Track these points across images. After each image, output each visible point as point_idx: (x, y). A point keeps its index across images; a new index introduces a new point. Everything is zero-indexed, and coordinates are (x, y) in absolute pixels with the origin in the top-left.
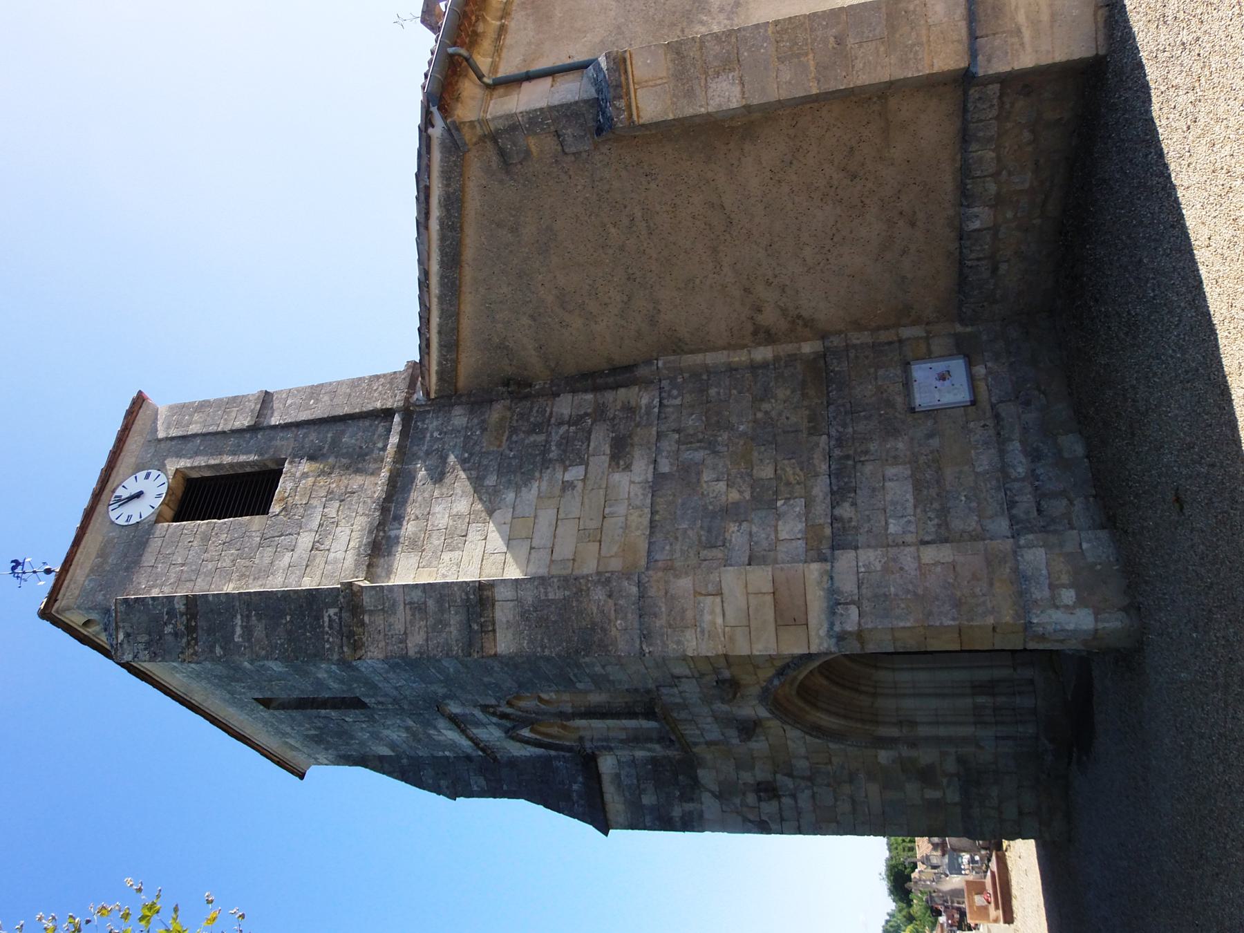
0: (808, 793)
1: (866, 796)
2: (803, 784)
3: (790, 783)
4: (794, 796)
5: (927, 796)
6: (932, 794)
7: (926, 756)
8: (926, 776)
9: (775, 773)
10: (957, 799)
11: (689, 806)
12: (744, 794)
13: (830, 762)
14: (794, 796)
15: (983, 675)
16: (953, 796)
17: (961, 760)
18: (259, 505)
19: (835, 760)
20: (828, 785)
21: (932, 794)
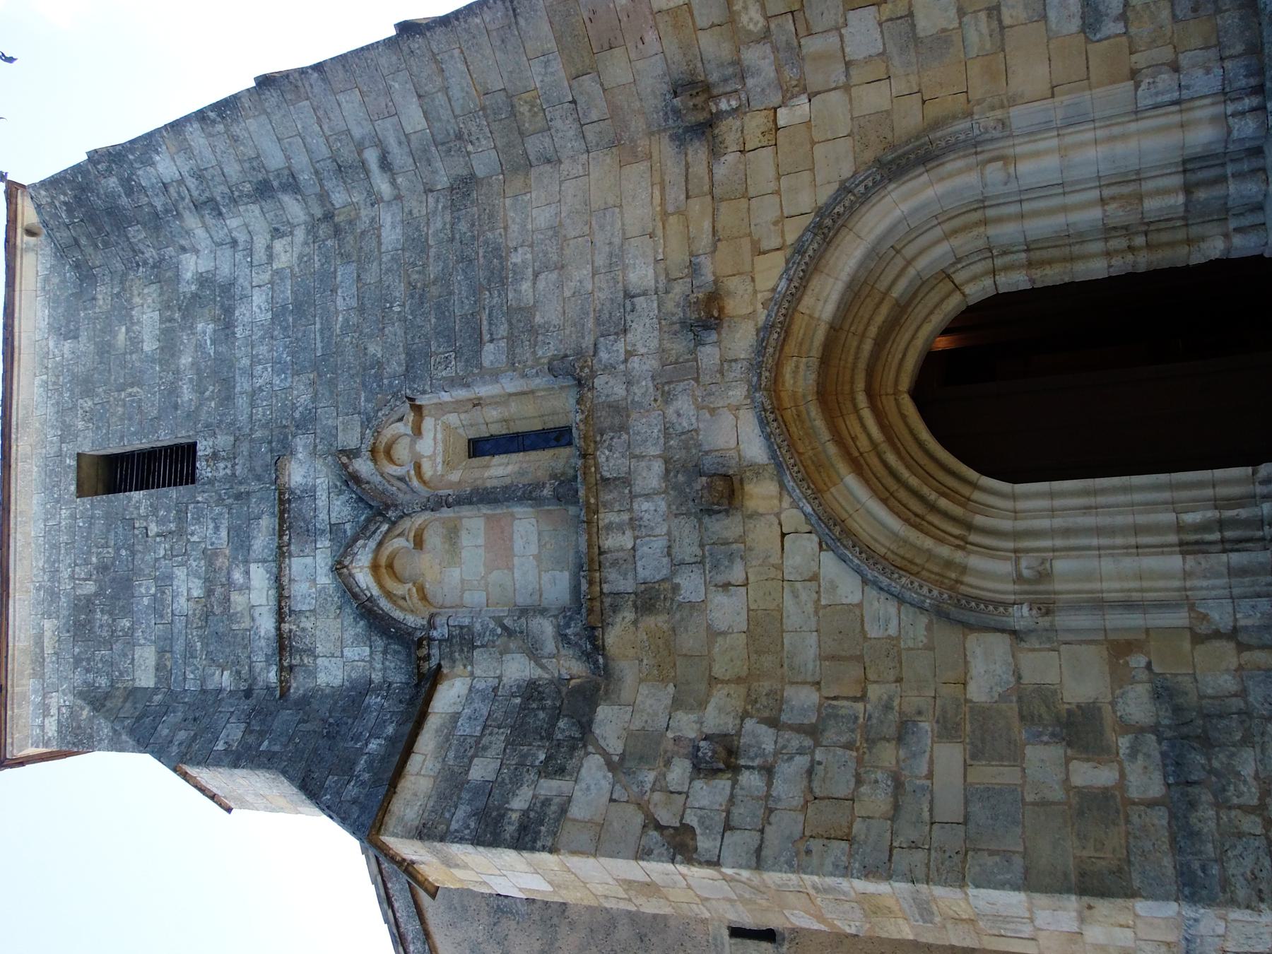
0: (802, 761)
1: (930, 776)
2: (796, 741)
3: (767, 739)
4: (768, 771)
5: (1077, 780)
6: (1092, 775)
7: (1079, 680)
8: (1079, 730)
9: (745, 715)
10: (1156, 789)
11: (550, 787)
12: (668, 763)
13: (863, 698)
14: (768, 771)
15: (1132, 541)
16: (1145, 780)
17: (1163, 692)
18: (189, 477)
19: (874, 692)
20: (849, 746)
21: (1092, 775)
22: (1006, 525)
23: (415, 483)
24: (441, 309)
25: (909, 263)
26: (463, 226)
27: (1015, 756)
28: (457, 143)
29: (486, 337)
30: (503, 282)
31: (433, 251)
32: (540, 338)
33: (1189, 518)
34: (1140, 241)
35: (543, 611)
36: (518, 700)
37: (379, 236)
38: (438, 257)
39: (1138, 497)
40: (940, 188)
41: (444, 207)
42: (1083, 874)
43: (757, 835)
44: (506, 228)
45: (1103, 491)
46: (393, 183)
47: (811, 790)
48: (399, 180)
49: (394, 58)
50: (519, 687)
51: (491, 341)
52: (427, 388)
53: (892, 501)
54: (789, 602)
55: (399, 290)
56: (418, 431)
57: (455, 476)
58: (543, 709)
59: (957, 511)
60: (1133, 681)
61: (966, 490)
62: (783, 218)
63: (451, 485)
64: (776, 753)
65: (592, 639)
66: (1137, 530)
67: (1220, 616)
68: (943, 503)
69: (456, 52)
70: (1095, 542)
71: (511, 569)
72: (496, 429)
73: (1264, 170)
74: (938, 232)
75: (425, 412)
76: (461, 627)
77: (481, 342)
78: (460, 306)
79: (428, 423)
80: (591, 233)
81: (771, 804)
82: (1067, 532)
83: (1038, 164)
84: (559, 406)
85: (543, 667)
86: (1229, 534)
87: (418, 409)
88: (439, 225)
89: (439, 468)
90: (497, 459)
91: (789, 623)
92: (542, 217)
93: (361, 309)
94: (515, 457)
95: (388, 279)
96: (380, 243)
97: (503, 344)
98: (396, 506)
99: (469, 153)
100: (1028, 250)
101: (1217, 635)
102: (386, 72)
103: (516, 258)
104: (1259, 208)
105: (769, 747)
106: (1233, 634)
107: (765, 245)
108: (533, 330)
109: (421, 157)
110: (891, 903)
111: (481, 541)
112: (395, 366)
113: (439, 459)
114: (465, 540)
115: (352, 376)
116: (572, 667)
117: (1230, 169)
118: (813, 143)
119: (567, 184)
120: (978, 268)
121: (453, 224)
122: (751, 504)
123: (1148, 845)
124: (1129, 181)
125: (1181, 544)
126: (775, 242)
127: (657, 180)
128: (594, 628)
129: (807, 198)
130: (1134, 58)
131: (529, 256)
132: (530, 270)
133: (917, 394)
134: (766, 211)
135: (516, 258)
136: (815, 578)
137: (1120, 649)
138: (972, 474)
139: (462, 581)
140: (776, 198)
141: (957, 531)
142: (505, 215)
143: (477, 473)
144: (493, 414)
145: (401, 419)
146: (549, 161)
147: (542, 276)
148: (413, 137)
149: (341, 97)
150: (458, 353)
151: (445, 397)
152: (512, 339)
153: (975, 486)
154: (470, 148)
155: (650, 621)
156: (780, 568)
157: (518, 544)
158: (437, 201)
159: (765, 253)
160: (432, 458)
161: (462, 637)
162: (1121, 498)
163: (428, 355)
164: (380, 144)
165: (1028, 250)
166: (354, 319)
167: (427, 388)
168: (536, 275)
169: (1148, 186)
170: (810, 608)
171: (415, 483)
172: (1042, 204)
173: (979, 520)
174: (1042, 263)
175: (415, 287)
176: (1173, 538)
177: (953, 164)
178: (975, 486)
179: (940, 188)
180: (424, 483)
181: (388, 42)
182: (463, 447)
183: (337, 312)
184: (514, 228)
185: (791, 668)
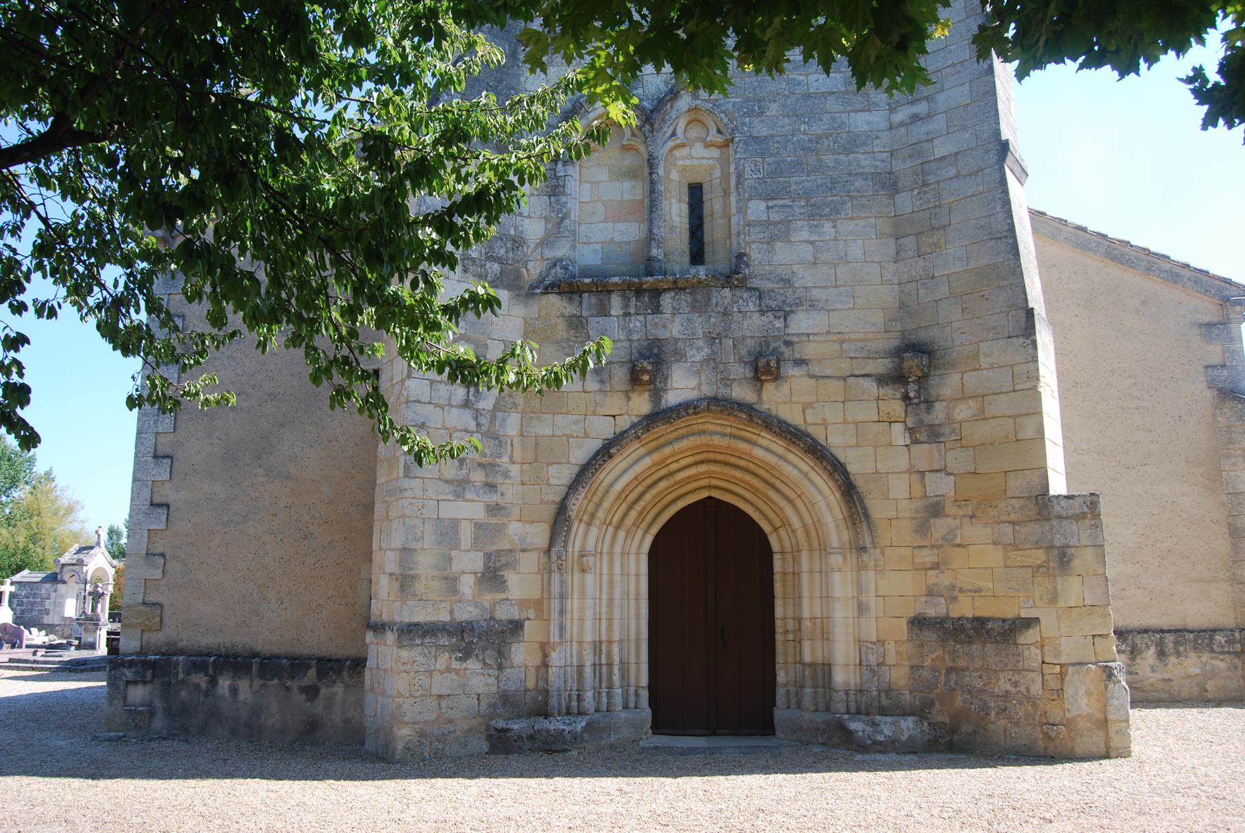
4: (466, 404)
6: (467, 585)
7: (521, 583)
14: (466, 404)
15: (604, 616)
21: (467, 585)
22: (618, 548)
23: (671, 144)
24: (798, 166)
25: (791, 502)
26: (859, 183)
27: (476, 544)
28: (920, 182)
29: (770, 203)
30: (811, 216)
31: (843, 157)
32: (765, 246)
33: (615, 649)
34: (791, 636)
35: (574, 247)
36: (512, 233)
37: (863, 111)
38: (837, 162)
39: (633, 622)
40: (831, 526)
41: (877, 167)
42: (413, 577)
43: (428, 400)
44: (851, 218)
45: (638, 604)
46: (902, 124)
47: (456, 430)
48: (902, 129)
49: (985, 136)
50: (522, 232)
51: (768, 208)
52: (738, 155)
53: (636, 482)
54: (571, 418)
55: (817, 129)
56: (708, 145)
57: (674, 175)
58: (507, 252)
59: (629, 521)
60: (521, 611)
61: (644, 526)
62: (824, 424)
63: (668, 173)
64: (477, 410)
65: (552, 285)
66: (610, 620)
67: (555, 657)
68: (633, 514)
69: (981, 188)
70: (604, 597)
71: (605, 221)
72: (707, 207)
73: (817, 710)
74: (808, 521)
75: (724, 150)
76: (564, 186)
77: (768, 198)
78: (798, 181)
79: (715, 153)
80: (837, 286)
81: (446, 408)
82: (611, 582)
83: (841, 585)
84: (718, 258)
85: (536, 248)
86: (604, 669)
87: (726, 144)
88: (863, 163)
89: (681, 162)
90: (685, 207)
91: (559, 418)
92: (855, 250)
93: (808, 96)
94: (686, 220)
95: (826, 118)
96: (856, 111)
97: (764, 217)
98: (652, 132)
99: (912, 190)
100: (794, 573)
101: (545, 656)
102: (978, 128)
103: (828, 226)
104: (799, 707)
105: (481, 405)
106: (545, 665)
107: (809, 411)
108: (771, 241)
109: (916, 150)
110: (394, 475)
111: (626, 197)
112: (761, 129)
113: (688, 162)
114: (627, 184)
115: (754, 90)
116: (534, 270)
117: (820, 690)
118: (875, 448)
119: (877, 267)
120: (786, 542)
121: (861, 174)
122: (634, 396)
123: (430, 610)
124: (825, 635)
125: (601, 642)
126: (810, 419)
127: (869, 336)
128: (559, 287)
129: (837, 441)
130: (892, 643)
131: (828, 237)
132: (816, 238)
133: (710, 497)
134: (832, 414)
135: (828, 226)
136: (586, 436)
137: (538, 604)
138: (655, 530)
139: (599, 182)
140: (841, 420)
141: (615, 520)
142: (862, 218)
143: (675, 192)
144: (718, 206)
145: (719, 131)
146: (897, 253)
147: (811, 247)
148: (930, 145)
149: (967, 87)
150: (762, 181)
151: (732, 168)
152: (768, 223)
153: (646, 531)
154: (916, 191)
155: (561, 325)
156: (594, 414)
157: (622, 226)
158: (883, 161)
159: (804, 412)
160: (690, 157)
161: (557, 187)
162: (633, 613)
163: (763, 156)
164: (929, 116)
165: (794, 573)
166: (799, 90)
167: (738, 155)
168: (812, 243)
169: (818, 644)
170: (567, 431)
171: (671, 144)
172: (817, 584)
173: (622, 534)
174: (784, 581)
175: (817, 143)
176: (604, 638)
177: (846, 535)
178: (646, 531)
179: (831, 526)
180: (671, 150)
181: (998, 132)
182: (696, 179)
183: (807, 75)
184: (851, 226)
185: (531, 418)
